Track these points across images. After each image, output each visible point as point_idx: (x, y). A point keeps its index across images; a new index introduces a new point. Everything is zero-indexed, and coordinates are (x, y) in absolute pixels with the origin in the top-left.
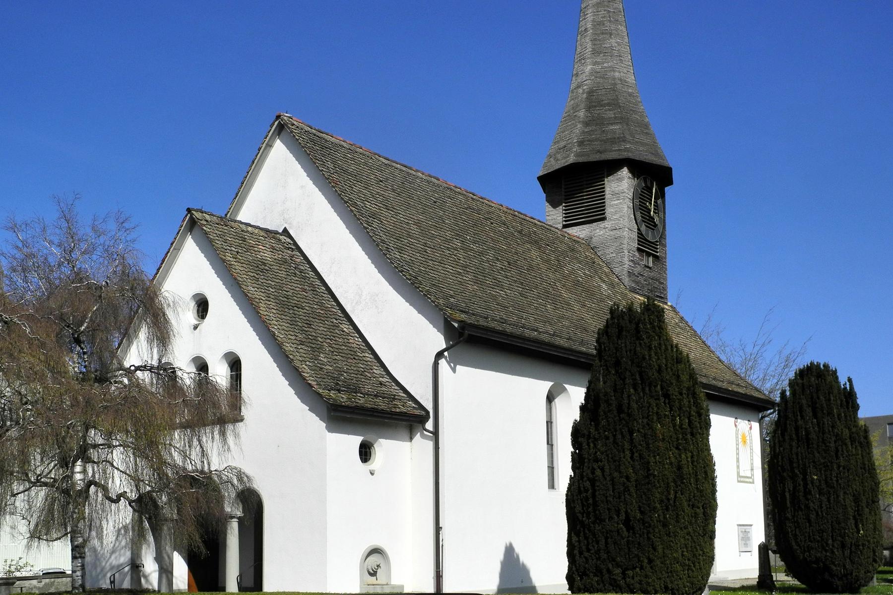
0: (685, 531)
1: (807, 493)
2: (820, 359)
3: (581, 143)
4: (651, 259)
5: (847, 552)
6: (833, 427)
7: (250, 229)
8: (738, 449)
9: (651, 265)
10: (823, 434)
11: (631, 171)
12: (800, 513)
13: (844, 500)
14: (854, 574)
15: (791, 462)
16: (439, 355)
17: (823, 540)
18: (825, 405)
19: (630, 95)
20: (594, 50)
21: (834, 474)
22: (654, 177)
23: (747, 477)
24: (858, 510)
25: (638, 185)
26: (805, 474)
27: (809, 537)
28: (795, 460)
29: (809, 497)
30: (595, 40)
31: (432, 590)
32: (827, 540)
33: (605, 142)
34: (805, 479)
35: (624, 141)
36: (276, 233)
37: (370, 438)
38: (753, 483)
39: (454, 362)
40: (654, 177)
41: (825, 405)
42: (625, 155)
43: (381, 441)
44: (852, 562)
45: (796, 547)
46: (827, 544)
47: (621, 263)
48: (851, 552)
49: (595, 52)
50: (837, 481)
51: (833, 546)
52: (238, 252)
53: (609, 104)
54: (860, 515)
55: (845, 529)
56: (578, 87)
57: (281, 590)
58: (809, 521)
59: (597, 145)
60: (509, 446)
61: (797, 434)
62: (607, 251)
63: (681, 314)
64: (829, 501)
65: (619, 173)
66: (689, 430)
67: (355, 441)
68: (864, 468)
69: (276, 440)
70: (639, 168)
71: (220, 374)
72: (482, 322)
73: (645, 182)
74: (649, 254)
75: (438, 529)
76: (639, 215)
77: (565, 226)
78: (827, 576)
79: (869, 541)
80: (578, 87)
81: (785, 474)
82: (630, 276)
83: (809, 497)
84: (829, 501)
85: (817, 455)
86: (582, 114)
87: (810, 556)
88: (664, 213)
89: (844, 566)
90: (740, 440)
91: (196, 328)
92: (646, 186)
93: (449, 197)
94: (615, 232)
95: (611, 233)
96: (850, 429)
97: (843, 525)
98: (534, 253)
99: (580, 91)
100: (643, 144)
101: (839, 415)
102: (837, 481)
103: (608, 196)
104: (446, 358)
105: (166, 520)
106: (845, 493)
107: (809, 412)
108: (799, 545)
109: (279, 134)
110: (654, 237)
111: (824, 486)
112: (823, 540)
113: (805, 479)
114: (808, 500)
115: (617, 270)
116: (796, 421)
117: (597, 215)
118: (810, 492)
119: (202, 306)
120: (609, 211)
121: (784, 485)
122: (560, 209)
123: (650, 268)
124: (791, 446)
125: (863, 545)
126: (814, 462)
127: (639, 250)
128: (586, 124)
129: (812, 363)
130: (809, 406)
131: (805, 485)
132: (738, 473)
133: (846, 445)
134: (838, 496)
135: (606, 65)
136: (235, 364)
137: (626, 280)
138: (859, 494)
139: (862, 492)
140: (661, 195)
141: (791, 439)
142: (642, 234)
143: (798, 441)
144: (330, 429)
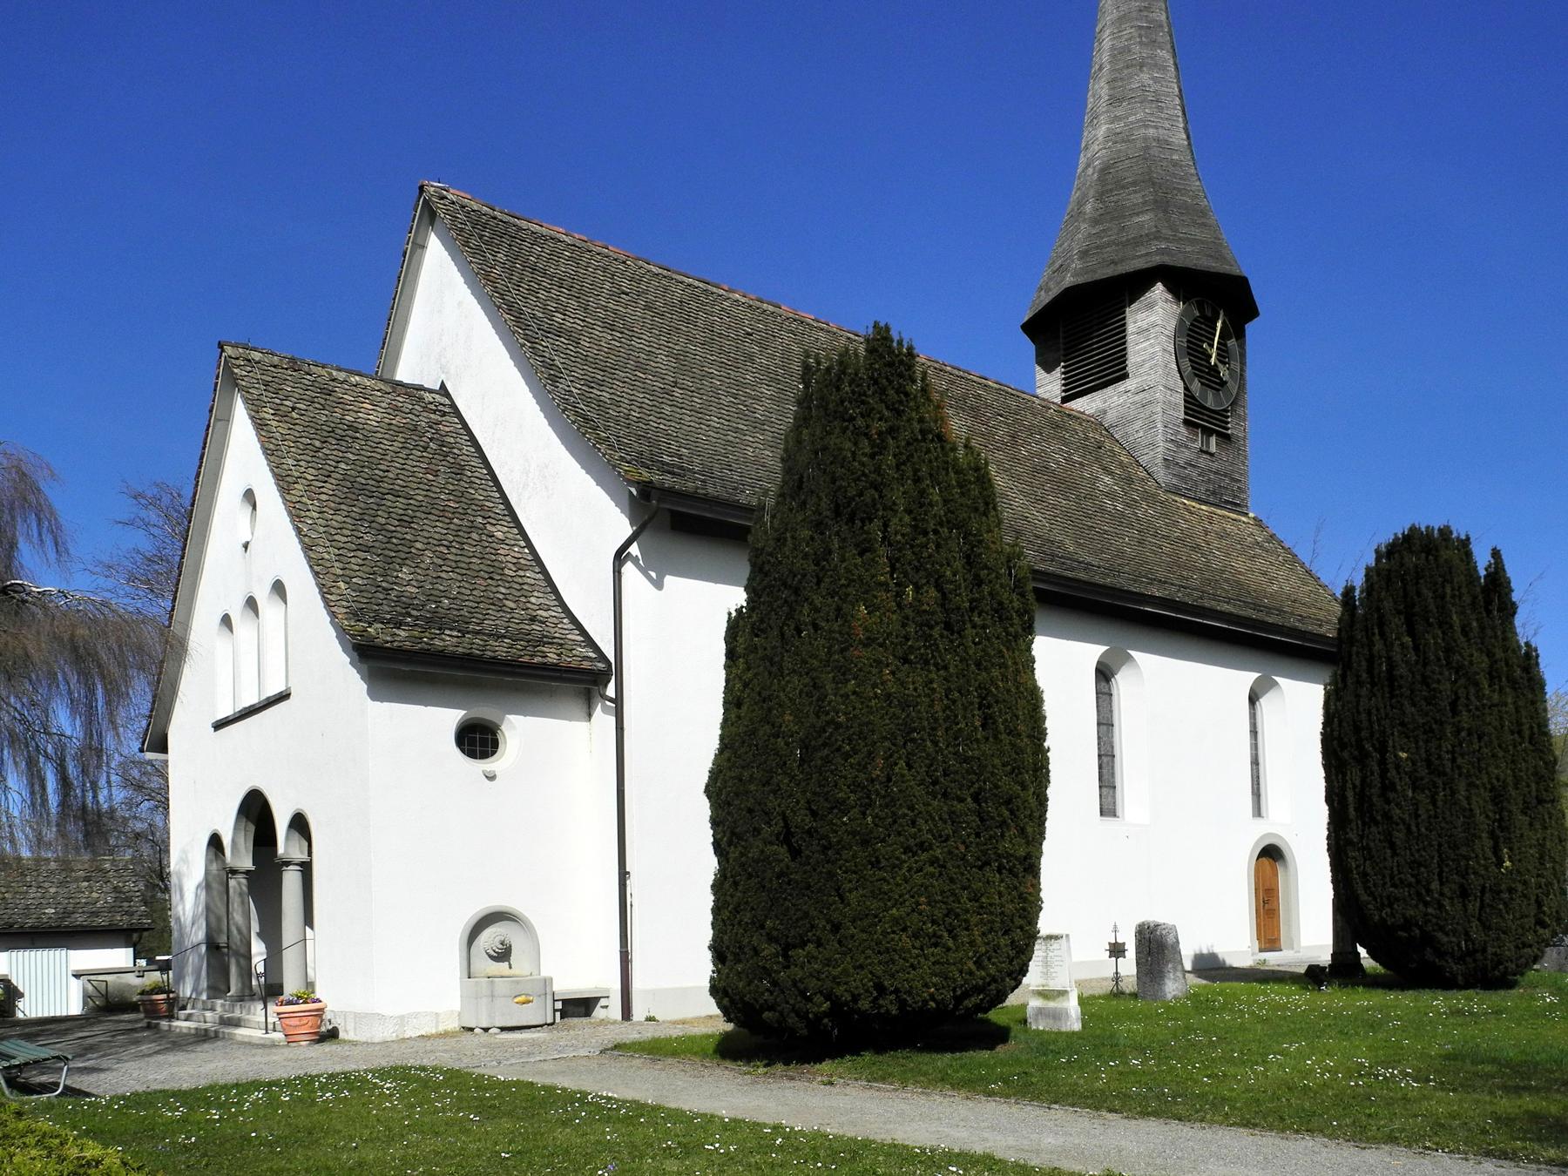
0: (924, 856)
1: (1387, 787)
2: (1430, 519)
3: (1084, 254)
4: (1213, 440)
5: (1474, 906)
6: (1449, 651)
9: (1213, 449)
10: (1425, 665)
11: (1170, 288)
12: (1374, 829)
13: (1468, 798)
14: (1490, 950)
15: (1357, 729)
16: (620, 557)
17: (1418, 882)
18: (1432, 607)
19: (1175, 164)
20: (1111, 97)
21: (1447, 746)
22: (1218, 303)
24: (1501, 819)
25: (1183, 314)
26: (1382, 749)
27: (1392, 878)
28: (1365, 724)
29: (1391, 795)
30: (1114, 80)
32: (1429, 883)
33: (1125, 244)
34: (1382, 762)
35: (1156, 238)
37: (484, 711)
39: (656, 570)
40: (1218, 303)
41: (1432, 607)
42: (1157, 260)
43: (511, 717)
44: (1486, 927)
45: (1364, 897)
46: (1429, 891)
48: (1482, 907)
49: (1115, 101)
50: (1454, 760)
51: (1442, 894)
53: (1134, 183)
54: (1502, 829)
55: (1468, 859)
56: (1088, 166)
58: (1392, 846)
61: (1370, 671)
62: (1129, 430)
63: (1272, 530)
64: (1434, 802)
66: (940, 616)
68: (1520, 733)
70: (1182, 282)
73: (1201, 309)
74: (1208, 432)
75: (623, 875)
76: (1186, 363)
77: (1065, 400)
78: (1429, 954)
79: (1525, 883)
80: (1088, 166)
81: (1346, 755)
82: (1167, 467)
83: (1391, 795)
84: (1434, 802)
85: (1409, 709)
87: (1393, 915)
88: (1243, 363)
89: (1467, 934)
92: (1203, 315)
94: (1142, 395)
95: (1137, 398)
96: (1490, 654)
97: (1463, 851)
99: (1090, 171)
100: (1193, 242)
101: (1465, 631)
102: (1454, 760)
103: (1131, 338)
104: (635, 561)
105: (288, 864)
106: (1471, 785)
107: (1396, 623)
108: (1371, 894)
109: (432, 223)
110: (1218, 401)
111: (1423, 772)
112: (1418, 882)
113: (1382, 762)
114: (1388, 802)
115: (1143, 460)
116: (1371, 644)
117: (1114, 371)
118: (1393, 785)
120: (1133, 359)
121: (1344, 775)
122: (1058, 373)
123: (1212, 455)
124: (1358, 696)
125: (1511, 890)
126: (1403, 724)
127: (1186, 422)
129: (1413, 529)
130: (1399, 612)
131: (1384, 772)
133: (1477, 684)
134: (1453, 793)
137: (1161, 475)
138: (1505, 786)
139: (1510, 780)
140: (1240, 335)
141: (1359, 683)
142: (1193, 397)
143: (1373, 684)
144: (374, 695)
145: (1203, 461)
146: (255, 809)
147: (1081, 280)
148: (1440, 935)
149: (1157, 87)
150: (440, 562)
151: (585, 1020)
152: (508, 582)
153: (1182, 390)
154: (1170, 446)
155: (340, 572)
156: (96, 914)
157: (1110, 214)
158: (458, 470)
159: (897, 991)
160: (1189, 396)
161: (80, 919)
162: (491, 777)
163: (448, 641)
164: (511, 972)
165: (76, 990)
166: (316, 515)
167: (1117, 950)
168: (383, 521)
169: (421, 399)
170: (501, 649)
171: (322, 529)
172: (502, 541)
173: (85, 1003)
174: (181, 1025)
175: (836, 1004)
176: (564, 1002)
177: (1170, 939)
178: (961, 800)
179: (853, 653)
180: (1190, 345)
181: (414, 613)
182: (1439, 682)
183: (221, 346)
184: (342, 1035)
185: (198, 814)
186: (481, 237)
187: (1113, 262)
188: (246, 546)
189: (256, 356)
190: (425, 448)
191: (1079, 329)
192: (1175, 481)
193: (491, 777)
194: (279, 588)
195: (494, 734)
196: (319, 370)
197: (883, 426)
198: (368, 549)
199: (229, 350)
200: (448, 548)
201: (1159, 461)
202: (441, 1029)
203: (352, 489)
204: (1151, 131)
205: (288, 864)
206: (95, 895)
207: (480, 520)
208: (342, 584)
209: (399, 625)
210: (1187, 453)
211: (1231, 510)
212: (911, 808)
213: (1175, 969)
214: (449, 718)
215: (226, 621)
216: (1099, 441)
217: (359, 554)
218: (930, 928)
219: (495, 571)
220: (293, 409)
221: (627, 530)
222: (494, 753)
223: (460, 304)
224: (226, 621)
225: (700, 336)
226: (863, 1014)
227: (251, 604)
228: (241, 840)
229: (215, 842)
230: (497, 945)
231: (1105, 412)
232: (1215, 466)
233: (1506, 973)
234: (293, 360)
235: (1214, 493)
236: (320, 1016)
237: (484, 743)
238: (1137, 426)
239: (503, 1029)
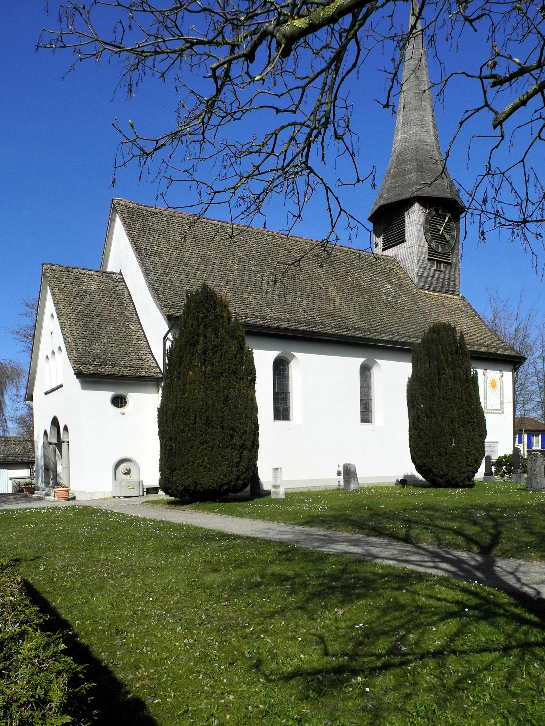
3: (388, 191)
9: (442, 269)
14: (450, 474)
22: (445, 209)
23: (499, 410)
30: (405, 116)
35: (416, 184)
38: (503, 413)
49: (405, 124)
53: (410, 160)
59: (398, 190)
63: (469, 301)
65: (413, 207)
70: (426, 202)
95: (408, 250)
103: (406, 225)
105: (64, 442)
115: (410, 276)
120: (407, 234)
123: (441, 271)
127: (429, 259)
135: (411, 132)
137: (416, 281)
144: (83, 388)
145: (437, 274)
146: (55, 422)
147: (386, 202)
148: (433, 469)
149: (422, 118)
150: (110, 340)
151: (156, 495)
152: (134, 346)
153: (427, 246)
154: (421, 270)
155: (74, 347)
156: (16, 457)
157: (400, 174)
158: (122, 304)
159: (200, 484)
160: (430, 248)
161: (11, 459)
162: (123, 414)
163: (107, 370)
164: (131, 478)
165: (10, 483)
166: (68, 326)
167: (339, 473)
168: (91, 326)
169: (112, 277)
170: (125, 372)
171: (70, 332)
172: (134, 331)
173: (13, 489)
174: (35, 496)
175: (185, 488)
176: (147, 489)
177: (353, 470)
178: (217, 429)
179: (187, 386)
180: (430, 228)
181: (97, 360)
182: (434, 380)
183: (42, 265)
184: (76, 499)
185: (41, 425)
186: (131, 218)
187: (399, 195)
188: (52, 333)
189: (54, 267)
190: (111, 297)
191: (388, 220)
192: (423, 284)
193: (123, 414)
194: (60, 348)
195: (125, 399)
196: (76, 270)
197: (202, 316)
198: (85, 338)
199: (45, 267)
200: (113, 334)
201: (415, 276)
202: (106, 497)
203: (83, 315)
204: (418, 138)
205: (64, 442)
206: (17, 450)
207: (127, 323)
208: (74, 351)
209: (91, 365)
210: (429, 271)
211: (451, 294)
212: (201, 431)
213: (354, 480)
214: (108, 395)
215: (47, 357)
216: (391, 270)
217: (82, 340)
218: (208, 466)
219: (129, 342)
220: (65, 287)
221: (167, 329)
222: (125, 406)
223: (125, 243)
224: (47, 357)
225: (213, 246)
226: (199, 491)
227: (53, 352)
228: (53, 432)
229: (45, 433)
230: (125, 470)
231: (397, 255)
232: (443, 276)
233: (456, 482)
234: (67, 267)
235: (442, 287)
236: (68, 492)
237: (121, 402)
238: (408, 262)
239: (125, 497)
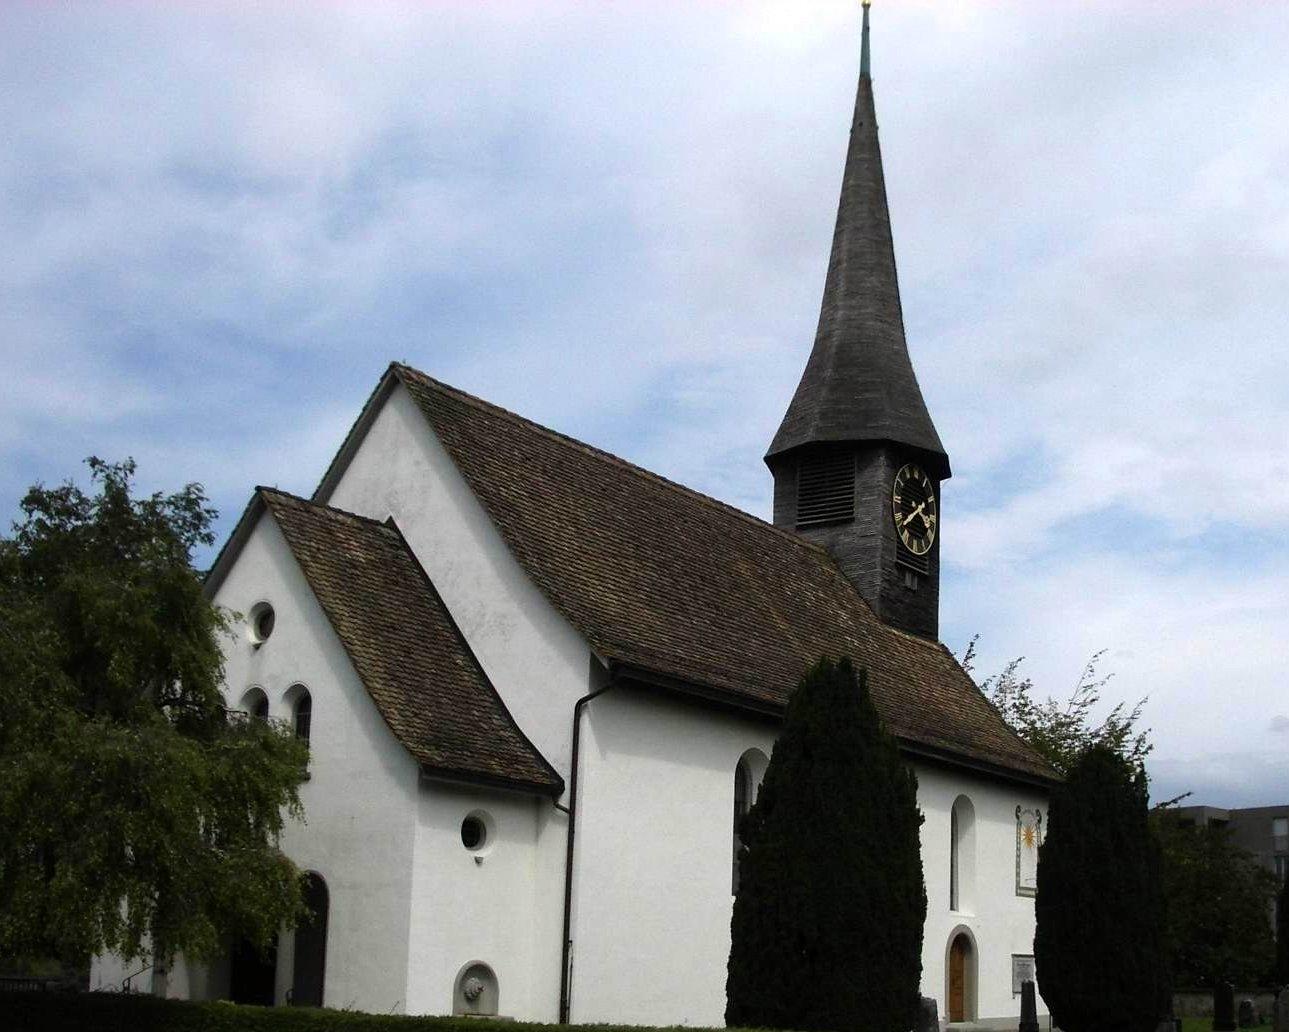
3: (823, 415)
7: (340, 517)
8: (1018, 849)
16: (580, 706)
31: (549, 1016)
36: (378, 523)
47: (872, 584)
52: (318, 549)
57: (723, 975)
60: (661, 836)
67: (458, 812)
69: (351, 804)
71: (280, 712)
72: (645, 662)
86: (828, 373)
90: (1023, 837)
91: (257, 647)
93: (627, 483)
98: (743, 567)
119: (264, 618)
120: (859, 512)
128: (833, 389)
132: (1018, 883)
136: (301, 700)
